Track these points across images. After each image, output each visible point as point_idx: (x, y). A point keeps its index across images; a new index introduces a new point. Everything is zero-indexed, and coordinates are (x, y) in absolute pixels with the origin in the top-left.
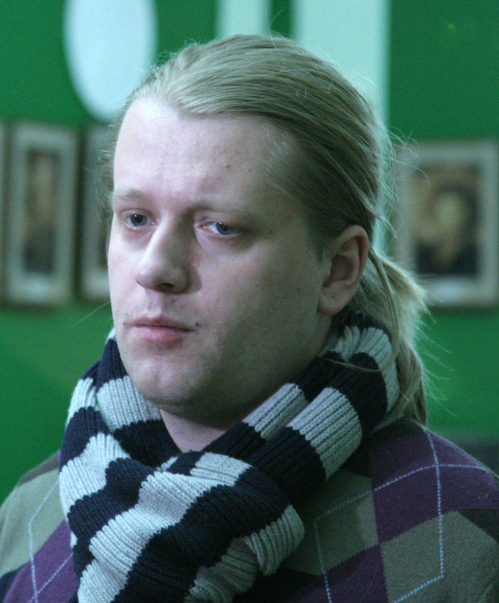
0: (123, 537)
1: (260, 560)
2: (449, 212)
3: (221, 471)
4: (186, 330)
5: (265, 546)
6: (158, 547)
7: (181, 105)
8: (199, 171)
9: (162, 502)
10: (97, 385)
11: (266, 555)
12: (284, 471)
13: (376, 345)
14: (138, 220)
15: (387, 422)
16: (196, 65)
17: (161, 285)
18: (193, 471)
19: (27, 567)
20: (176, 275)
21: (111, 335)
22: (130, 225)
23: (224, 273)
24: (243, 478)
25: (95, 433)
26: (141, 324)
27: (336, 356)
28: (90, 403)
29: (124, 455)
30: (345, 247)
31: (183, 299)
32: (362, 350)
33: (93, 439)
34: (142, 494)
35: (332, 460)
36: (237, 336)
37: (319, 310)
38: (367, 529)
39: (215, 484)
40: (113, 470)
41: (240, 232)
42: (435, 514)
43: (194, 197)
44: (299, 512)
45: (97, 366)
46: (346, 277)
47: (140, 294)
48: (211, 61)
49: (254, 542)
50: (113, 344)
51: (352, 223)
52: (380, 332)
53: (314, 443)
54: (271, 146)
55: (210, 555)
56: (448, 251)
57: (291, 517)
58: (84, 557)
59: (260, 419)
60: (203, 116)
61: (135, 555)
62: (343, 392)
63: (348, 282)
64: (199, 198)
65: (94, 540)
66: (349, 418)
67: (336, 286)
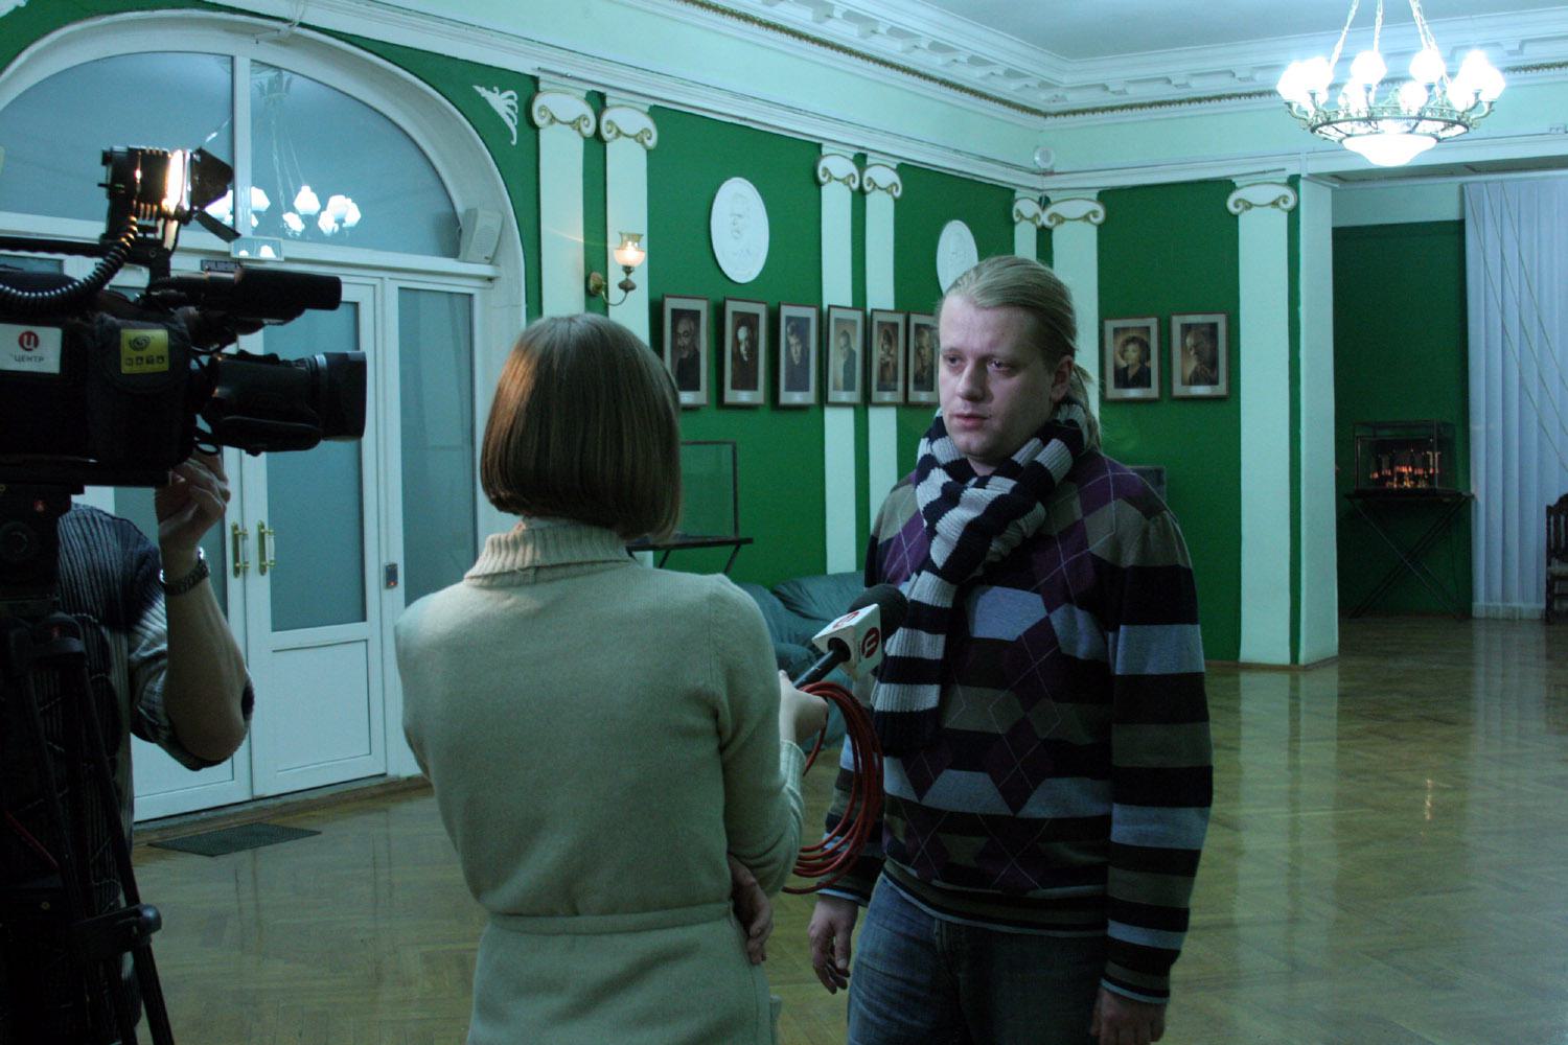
0: (954, 520)
1: (1025, 530)
2: (1133, 352)
3: (1001, 486)
4: (985, 418)
5: (1028, 523)
6: (971, 528)
7: (976, 302)
8: (988, 337)
9: (972, 504)
10: (931, 441)
11: (1028, 527)
12: (1034, 484)
13: (1077, 415)
14: (953, 360)
15: (1085, 452)
16: (981, 278)
17: (971, 397)
18: (987, 486)
19: (899, 535)
20: (978, 392)
21: (938, 414)
22: (949, 363)
23: (1002, 387)
24: (1014, 489)
25: (933, 468)
26: (959, 416)
27: (1058, 421)
28: (928, 451)
29: (950, 480)
30: (1062, 366)
31: (982, 405)
32: (1070, 417)
33: (932, 471)
34: (962, 500)
35: (1058, 476)
36: (1011, 417)
37: (1050, 399)
38: (1078, 514)
39: (1000, 493)
40: (945, 487)
41: (1011, 367)
42: (1110, 501)
43: (986, 351)
44: (1043, 504)
45: (931, 430)
46: (1062, 381)
47: (959, 402)
48: (989, 275)
49: (1021, 522)
50: (940, 420)
51: (1065, 354)
52: (1079, 407)
53: (1049, 468)
54: (1023, 320)
55: (999, 531)
56: (1131, 373)
57: (1039, 508)
58: (932, 532)
59: (1020, 457)
60: (987, 309)
61: (960, 532)
62: (1062, 440)
63: (1064, 384)
64: (989, 351)
65: (938, 525)
66: (1067, 455)
67: (1058, 387)
